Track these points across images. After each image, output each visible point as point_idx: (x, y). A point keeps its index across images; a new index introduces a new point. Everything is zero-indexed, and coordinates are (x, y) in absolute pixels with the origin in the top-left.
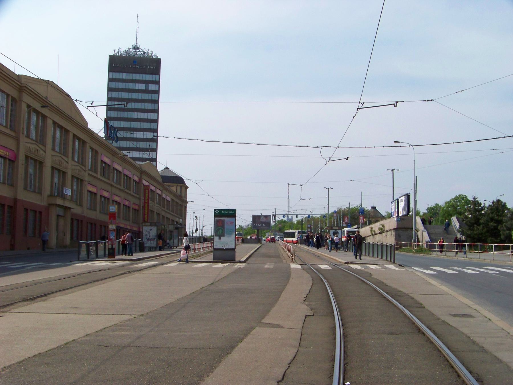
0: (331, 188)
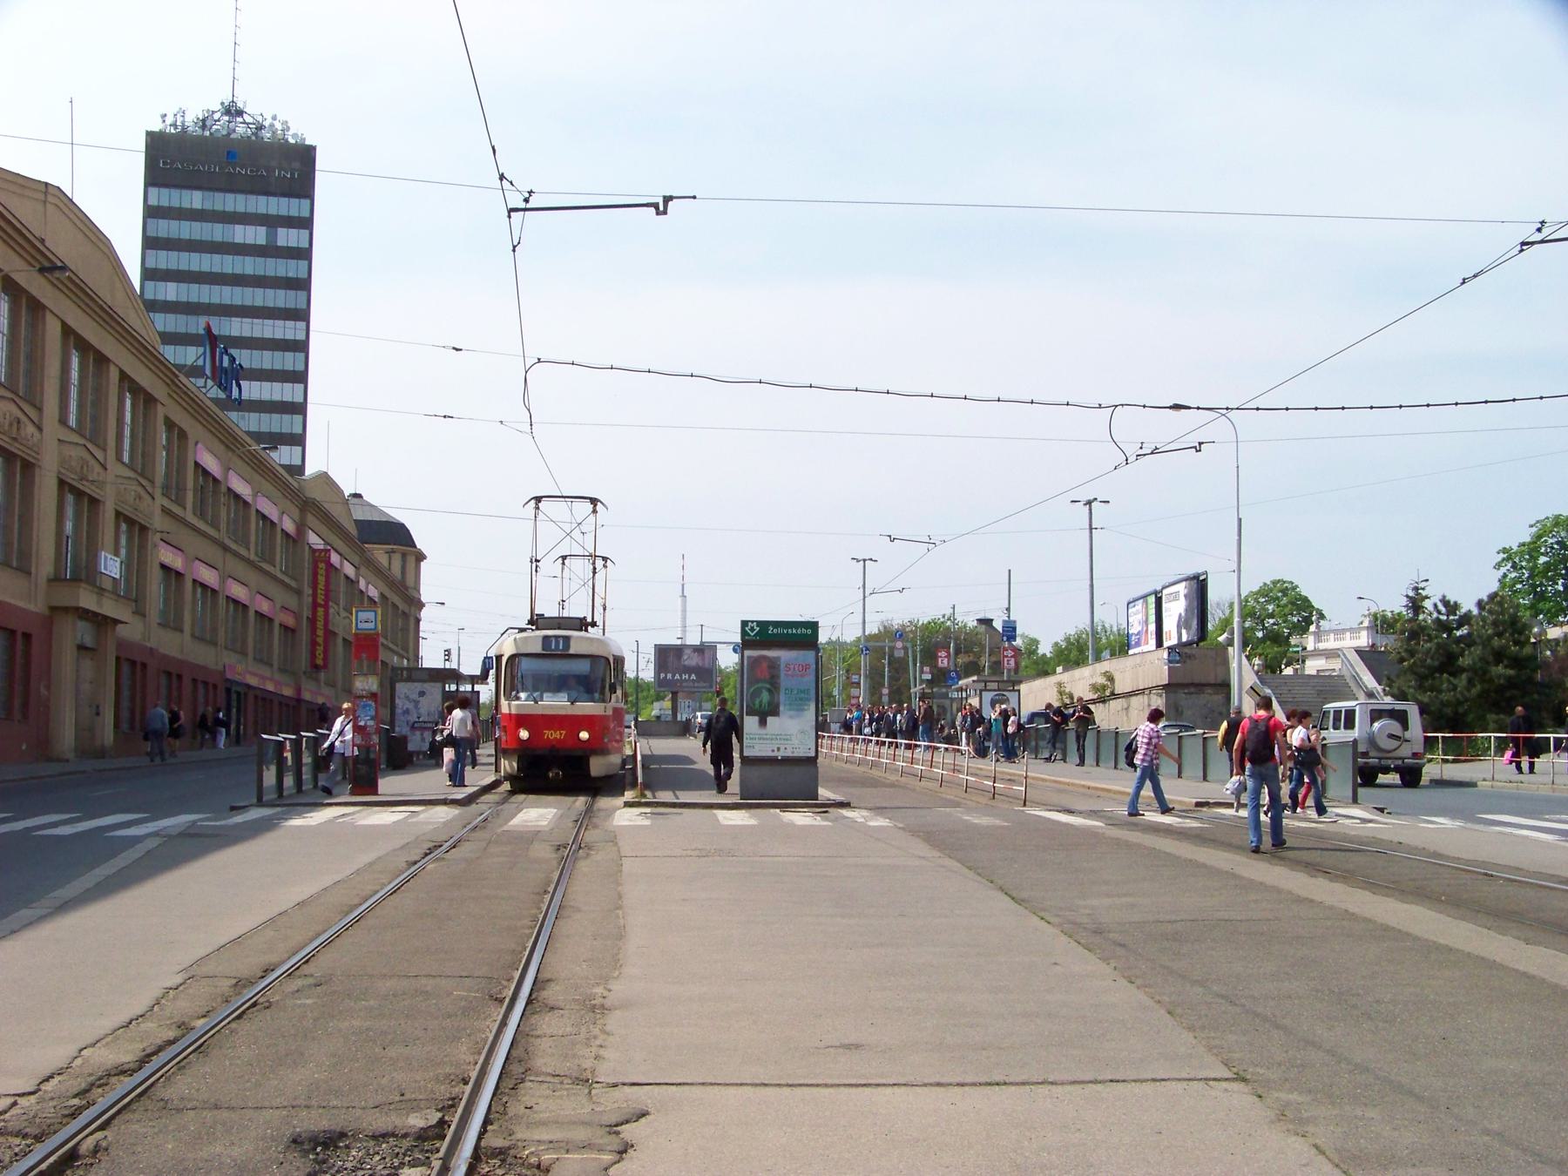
0: (871, 559)
